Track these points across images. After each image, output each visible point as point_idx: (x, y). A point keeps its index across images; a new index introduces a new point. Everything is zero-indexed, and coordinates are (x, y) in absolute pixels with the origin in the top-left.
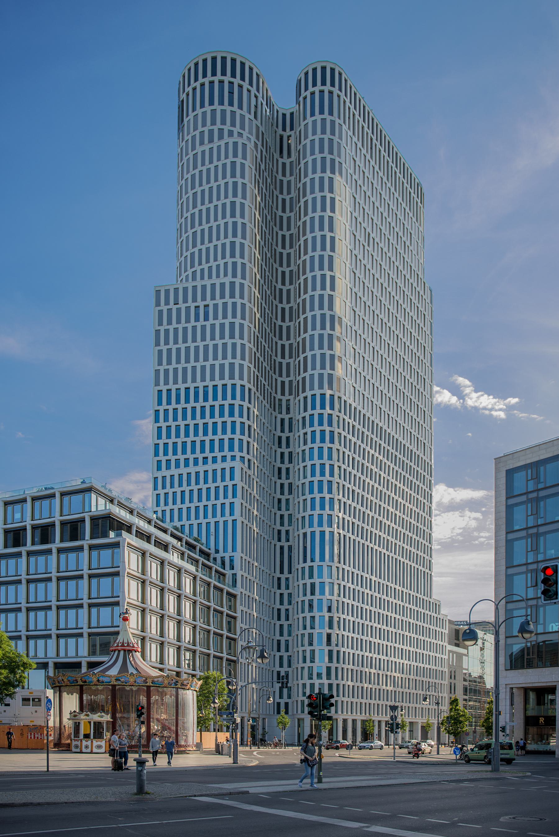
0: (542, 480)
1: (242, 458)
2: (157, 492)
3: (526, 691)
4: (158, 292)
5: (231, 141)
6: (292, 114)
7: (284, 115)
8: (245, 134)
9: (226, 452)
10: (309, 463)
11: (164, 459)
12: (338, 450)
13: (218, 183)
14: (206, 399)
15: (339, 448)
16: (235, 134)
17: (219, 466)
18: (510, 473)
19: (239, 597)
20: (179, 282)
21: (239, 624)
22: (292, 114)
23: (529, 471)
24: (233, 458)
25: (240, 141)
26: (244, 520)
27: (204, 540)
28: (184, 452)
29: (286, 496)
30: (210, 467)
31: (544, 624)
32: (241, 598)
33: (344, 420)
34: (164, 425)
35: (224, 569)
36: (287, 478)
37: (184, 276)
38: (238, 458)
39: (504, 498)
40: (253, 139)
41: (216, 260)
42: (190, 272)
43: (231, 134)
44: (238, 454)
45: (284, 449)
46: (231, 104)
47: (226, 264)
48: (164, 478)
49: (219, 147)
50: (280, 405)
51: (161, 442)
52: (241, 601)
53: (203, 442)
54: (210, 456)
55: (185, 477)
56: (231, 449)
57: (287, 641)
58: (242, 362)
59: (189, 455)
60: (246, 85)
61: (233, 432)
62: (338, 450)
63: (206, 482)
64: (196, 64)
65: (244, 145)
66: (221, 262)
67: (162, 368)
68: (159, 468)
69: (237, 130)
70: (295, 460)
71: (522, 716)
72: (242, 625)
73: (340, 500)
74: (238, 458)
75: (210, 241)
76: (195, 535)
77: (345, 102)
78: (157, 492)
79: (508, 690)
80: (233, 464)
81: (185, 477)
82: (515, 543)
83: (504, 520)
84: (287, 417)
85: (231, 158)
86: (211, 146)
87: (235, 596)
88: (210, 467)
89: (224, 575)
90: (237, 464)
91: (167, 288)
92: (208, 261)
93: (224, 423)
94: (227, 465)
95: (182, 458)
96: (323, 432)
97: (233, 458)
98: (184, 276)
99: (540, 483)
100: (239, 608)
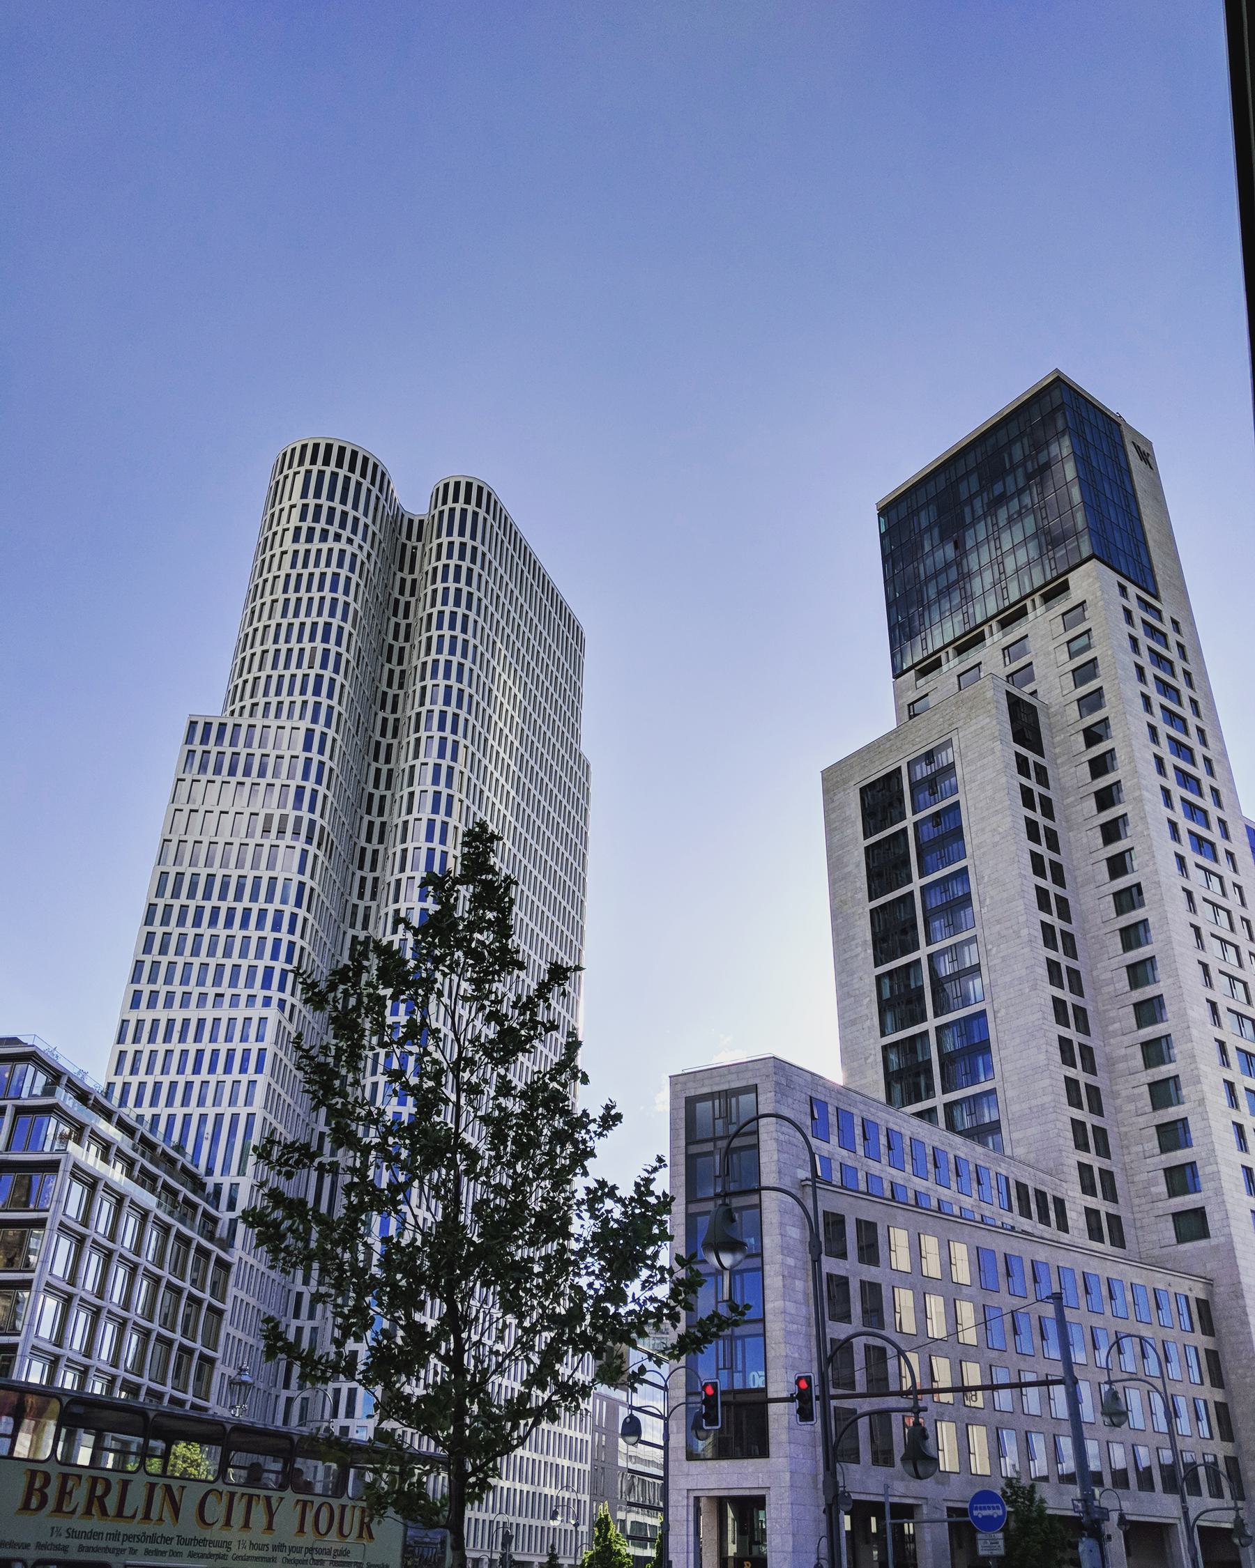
0: (734, 1120)
1: (282, 1003)
2: (122, 1047)
3: (721, 1503)
4: (193, 724)
5: (337, 547)
6: (421, 522)
7: (411, 522)
8: (357, 540)
9: (257, 990)
10: (435, 633)
11: (146, 988)
12: (462, 773)
13: (310, 595)
14: (238, 897)
15: (458, 824)
16: (344, 539)
17: (240, 1013)
18: (691, 1102)
19: (234, 1269)
20: (228, 713)
21: (226, 1328)
22: (421, 522)
23: (717, 1102)
24: (267, 1001)
25: (349, 550)
26: (278, 1052)
27: (189, 1149)
28: (185, 981)
29: (407, 597)
30: (224, 1013)
31: (744, 1372)
32: (239, 1268)
33: (469, 779)
34: (159, 930)
35: (217, 1209)
36: (373, 869)
37: (238, 705)
38: (275, 1002)
39: (683, 1143)
40: (367, 547)
41: (309, 590)
42: (248, 702)
43: (338, 537)
44: (275, 995)
45: (381, 764)
46: (343, 501)
47: (322, 599)
48: (140, 1022)
49: (319, 551)
50: (354, 914)
51: (148, 959)
52: (238, 1276)
53: (220, 967)
54: (229, 993)
55: (178, 1027)
56: (266, 984)
57: (368, 908)
58: (326, 730)
59: (192, 987)
60: (366, 484)
61: (332, 614)
62: (462, 773)
63: (213, 1039)
64: (304, 447)
65: (354, 556)
66: (316, 596)
67: (148, 959)
68: (135, 1004)
69: (346, 533)
70: (389, 837)
71: (714, 1462)
72: (232, 1330)
73: (461, 801)
74: (275, 1002)
75: (287, 667)
76: (176, 1137)
77: (487, 582)
78: (122, 1047)
79: (691, 1501)
80: (265, 1012)
81: (178, 1027)
82: (699, 1218)
83: (683, 1124)
84: (370, 877)
85: (317, 669)
86: (308, 546)
87: (224, 1266)
88: (224, 1013)
89: (215, 1221)
90: (272, 1013)
91: (208, 720)
92: (278, 693)
93: (262, 940)
94: (256, 1012)
95: (179, 990)
96: (454, 639)
97: (267, 1001)
98: (238, 705)
99: (731, 1123)
100: (232, 1291)
